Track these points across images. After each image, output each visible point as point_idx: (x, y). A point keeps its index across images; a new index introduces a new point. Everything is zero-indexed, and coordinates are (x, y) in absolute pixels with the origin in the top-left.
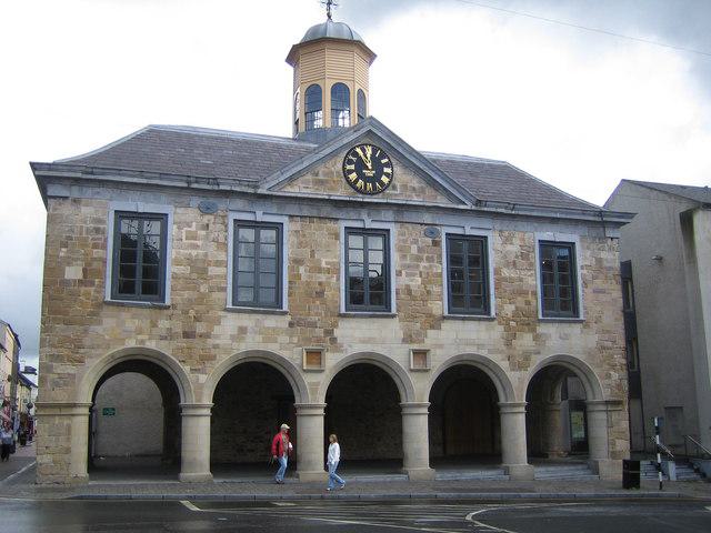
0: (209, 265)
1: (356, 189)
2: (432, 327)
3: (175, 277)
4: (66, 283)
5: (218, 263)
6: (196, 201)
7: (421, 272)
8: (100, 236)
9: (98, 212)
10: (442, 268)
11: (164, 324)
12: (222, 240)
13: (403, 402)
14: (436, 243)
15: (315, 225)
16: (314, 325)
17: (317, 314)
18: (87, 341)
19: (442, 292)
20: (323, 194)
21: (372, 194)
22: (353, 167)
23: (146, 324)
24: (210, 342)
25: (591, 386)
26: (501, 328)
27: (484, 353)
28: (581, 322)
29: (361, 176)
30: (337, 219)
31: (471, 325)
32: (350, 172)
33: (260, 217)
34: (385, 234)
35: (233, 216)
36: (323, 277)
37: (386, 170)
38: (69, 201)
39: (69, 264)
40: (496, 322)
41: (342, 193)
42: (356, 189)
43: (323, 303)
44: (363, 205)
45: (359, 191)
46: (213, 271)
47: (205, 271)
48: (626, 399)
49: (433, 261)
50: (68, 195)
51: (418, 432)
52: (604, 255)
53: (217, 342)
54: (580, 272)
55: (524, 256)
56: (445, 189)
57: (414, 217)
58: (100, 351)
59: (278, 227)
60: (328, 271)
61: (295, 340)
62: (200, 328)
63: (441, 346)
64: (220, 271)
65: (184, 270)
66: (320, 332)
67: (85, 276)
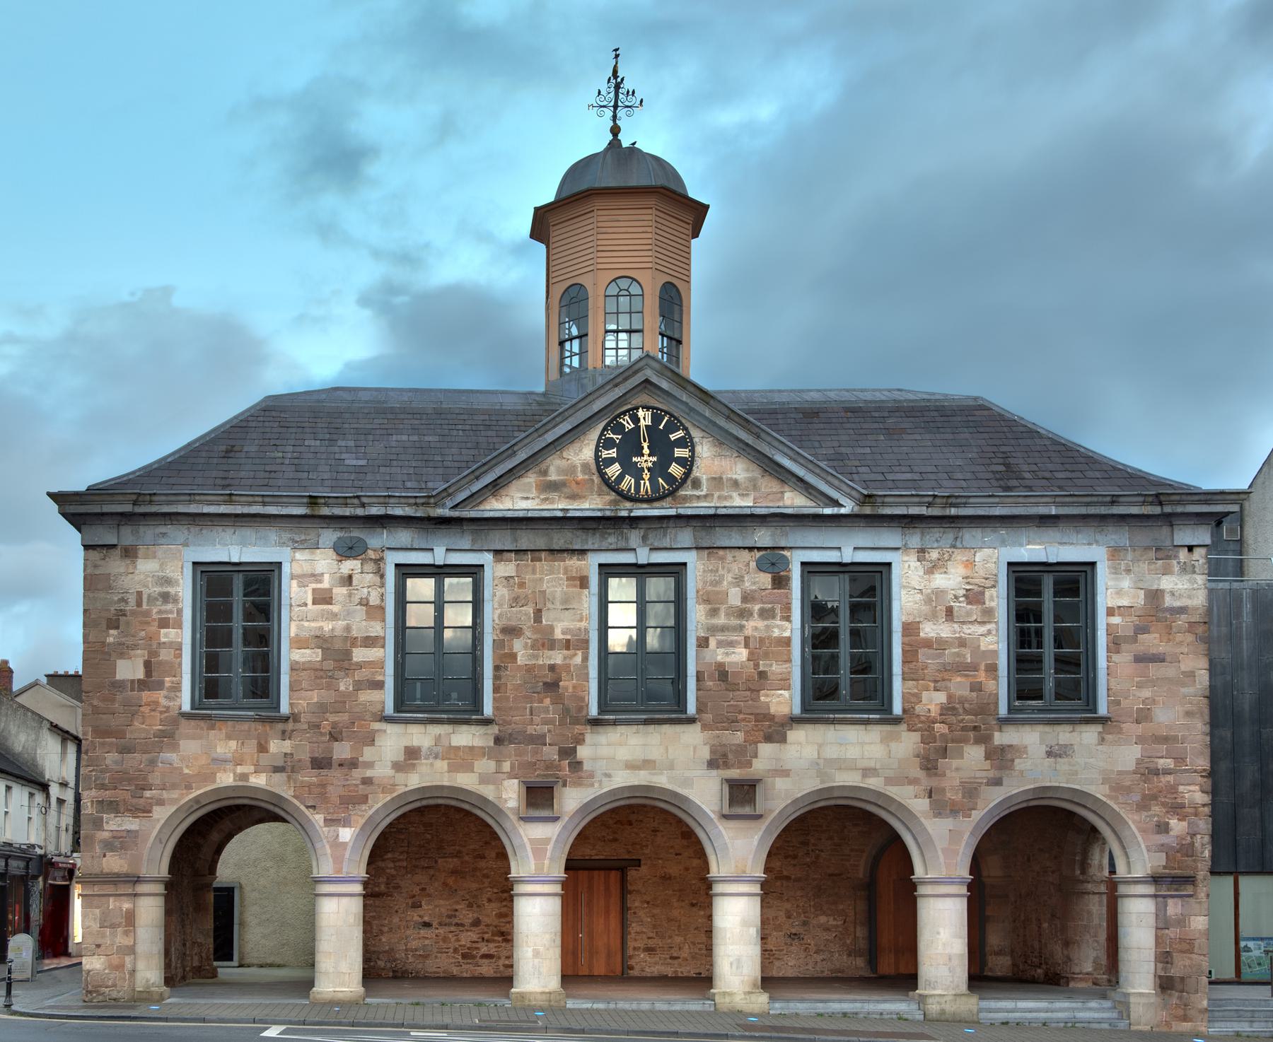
0: (354, 645)
1: (602, 475)
2: (769, 739)
3: (294, 667)
4: (120, 685)
5: (370, 642)
6: (330, 536)
7: (747, 639)
8: (169, 607)
10: (792, 628)
11: (277, 747)
12: (374, 600)
13: (513, 874)
14: (780, 582)
15: (543, 565)
16: (539, 740)
17: (545, 722)
18: (155, 778)
20: (558, 505)
21: (649, 500)
22: (613, 453)
23: (252, 746)
24: (357, 774)
25: (1124, 848)
26: (915, 737)
27: (874, 783)
28: (1103, 721)
31: (852, 734)
32: (610, 461)
33: (440, 556)
34: (676, 571)
35: (393, 559)
36: (557, 657)
37: (680, 452)
38: (118, 552)
39: (122, 655)
41: (592, 504)
42: (602, 475)
43: (558, 700)
44: (634, 521)
45: (625, 496)
46: (359, 655)
47: (347, 655)
49: (774, 617)
50: (114, 542)
52: (1166, 583)
53: (369, 773)
54: (1102, 621)
55: (974, 597)
56: (801, 480)
57: (734, 537)
58: (175, 794)
59: (474, 572)
60: (567, 645)
61: (506, 766)
63: (785, 773)
64: (373, 654)
65: (310, 655)
66: (551, 753)
67: (95, 652)
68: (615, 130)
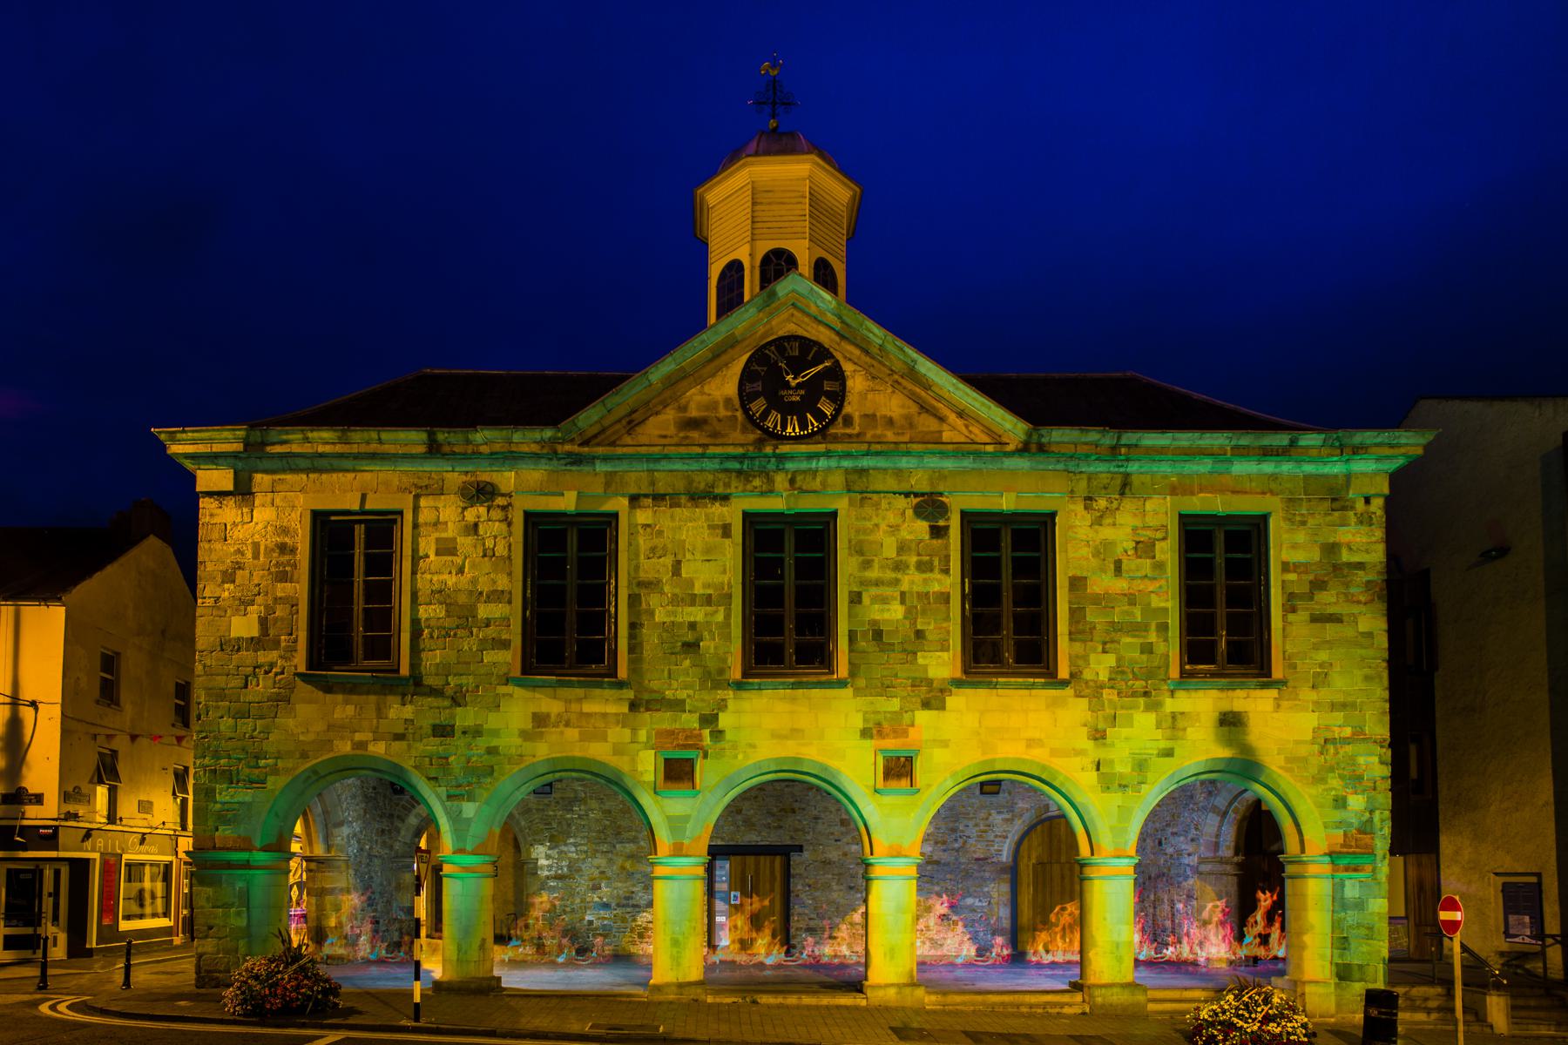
0: (478, 600)
2: (926, 705)
11: (399, 711)
12: (501, 550)
24: (482, 743)
36: (697, 614)
46: (484, 611)
66: (690, 721)
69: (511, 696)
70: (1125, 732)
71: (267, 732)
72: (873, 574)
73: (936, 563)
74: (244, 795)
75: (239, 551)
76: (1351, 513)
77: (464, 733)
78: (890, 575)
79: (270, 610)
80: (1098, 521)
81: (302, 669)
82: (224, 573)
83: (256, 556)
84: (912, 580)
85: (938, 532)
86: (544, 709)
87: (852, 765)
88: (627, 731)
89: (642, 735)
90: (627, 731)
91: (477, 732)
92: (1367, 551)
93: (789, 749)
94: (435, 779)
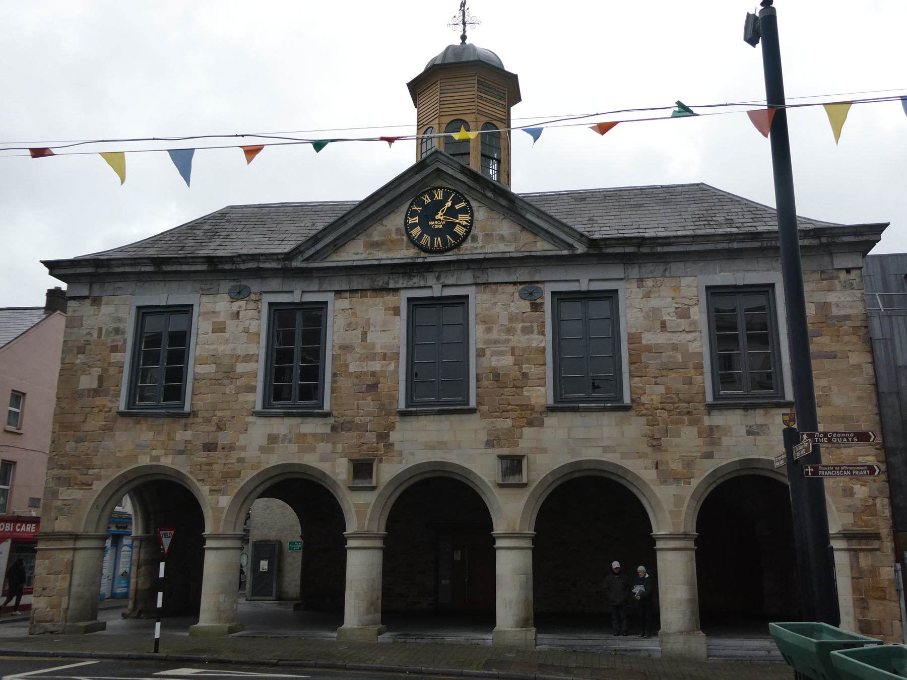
0: (237, 361)
2: (530, 424)
5: (248, 358)
9: (118, 312)
11: (182, 435)
12: (253, 329)
15: (370, 300)
16: (363, 428)
19: (396, 371)
21: (441, 252)
24: (234, 456)
29: (426, 229)
30: (397, 290)
32: (414, 226)
36: (376, 366)
39: (84, 372)
40: (632, 413)
41: (404, 254)
46: (241, 368)
48: (885, 530)
51: (675, 577)
53: (243, 454)
56: (547, 232)
62: (224, 438)
66: (371, 437)
68: (464, 38)
69: (255, 423)
70: (675, 441)
71: (96, 450)
72: (494, 335)
73: (535, 327)
74: (76, 494)
75: (89, 334)
76: (837, 281)
77: (223, 448)
78: (503, 336)
79: (105, 370)
80: (647, 296)
81: (122, 408)
82: (79, 347)
83: (100, 336)
84: (520, 340)
85: (536, 307)
86: (275, 431)
87: (483, 467)
88: (330, 445)
89: (339, 447)
90: (330, 445)
91: (232, 448)
92: (851, 307)
93: (438, 456)
94: (203, 480)
